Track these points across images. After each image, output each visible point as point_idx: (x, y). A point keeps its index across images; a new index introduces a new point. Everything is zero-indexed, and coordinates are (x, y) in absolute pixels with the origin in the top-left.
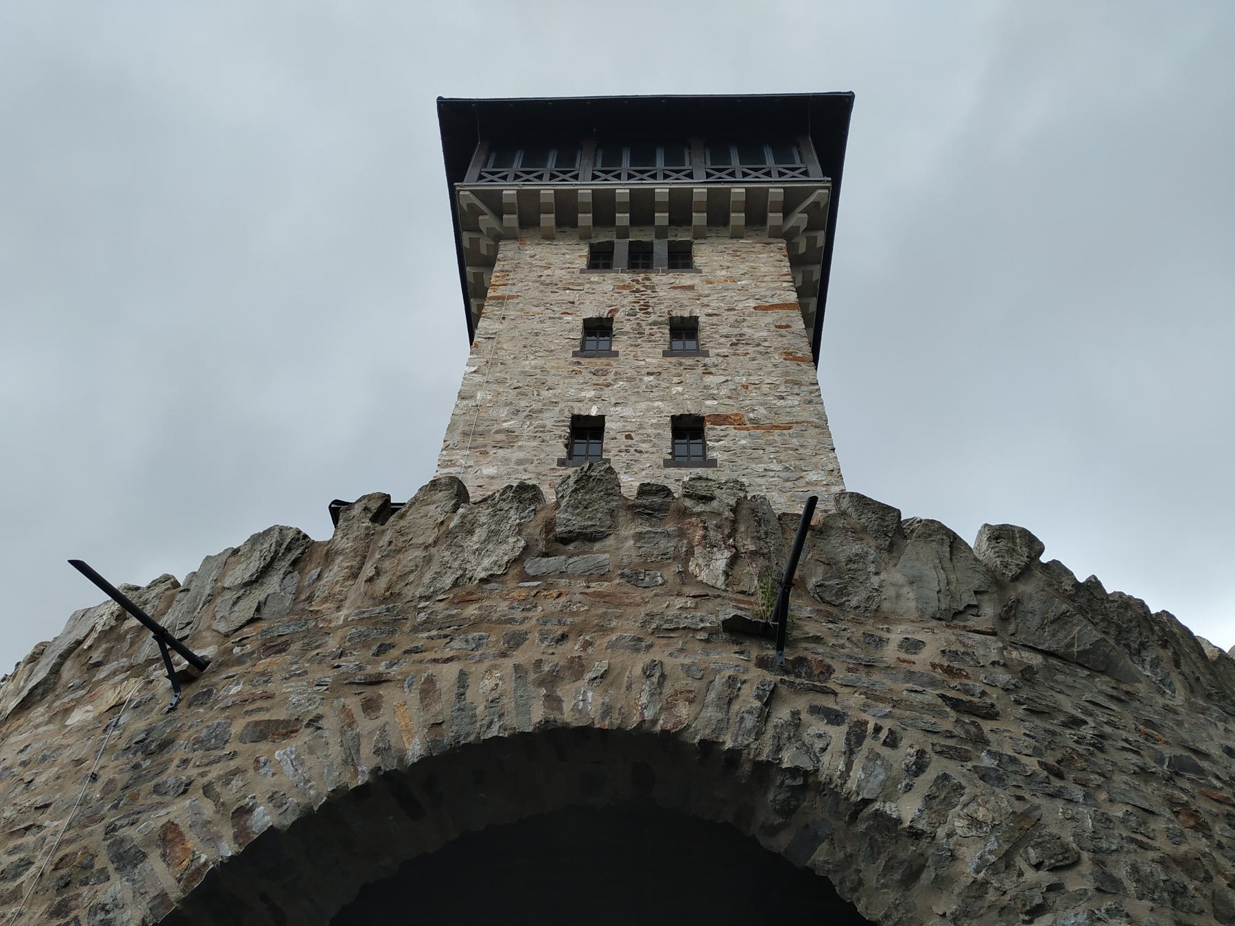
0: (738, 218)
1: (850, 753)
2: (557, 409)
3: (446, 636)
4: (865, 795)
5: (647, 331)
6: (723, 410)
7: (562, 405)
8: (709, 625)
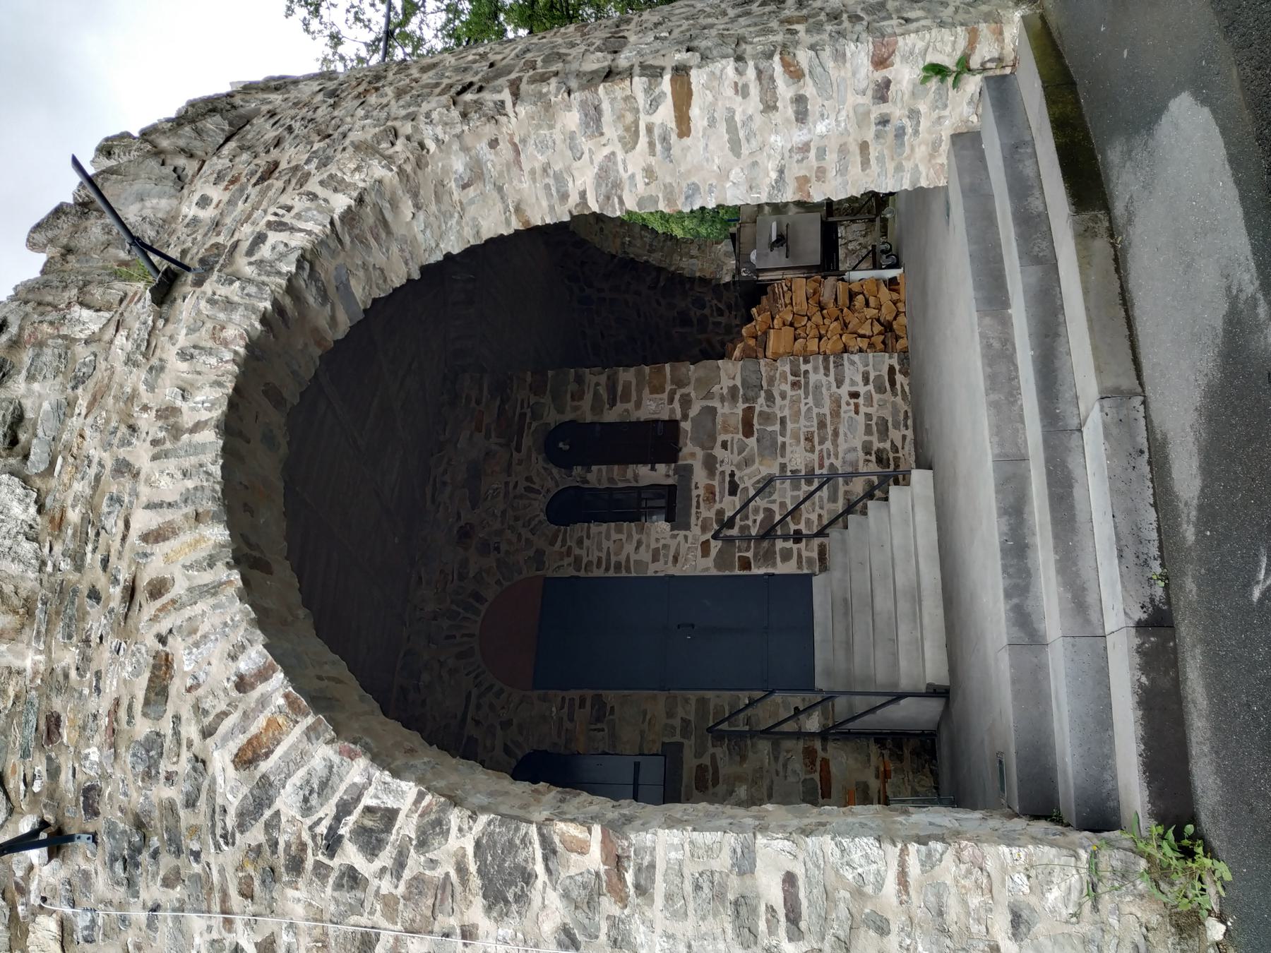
1: (292, 229)
3: (98, 534)
8: (151, 318)
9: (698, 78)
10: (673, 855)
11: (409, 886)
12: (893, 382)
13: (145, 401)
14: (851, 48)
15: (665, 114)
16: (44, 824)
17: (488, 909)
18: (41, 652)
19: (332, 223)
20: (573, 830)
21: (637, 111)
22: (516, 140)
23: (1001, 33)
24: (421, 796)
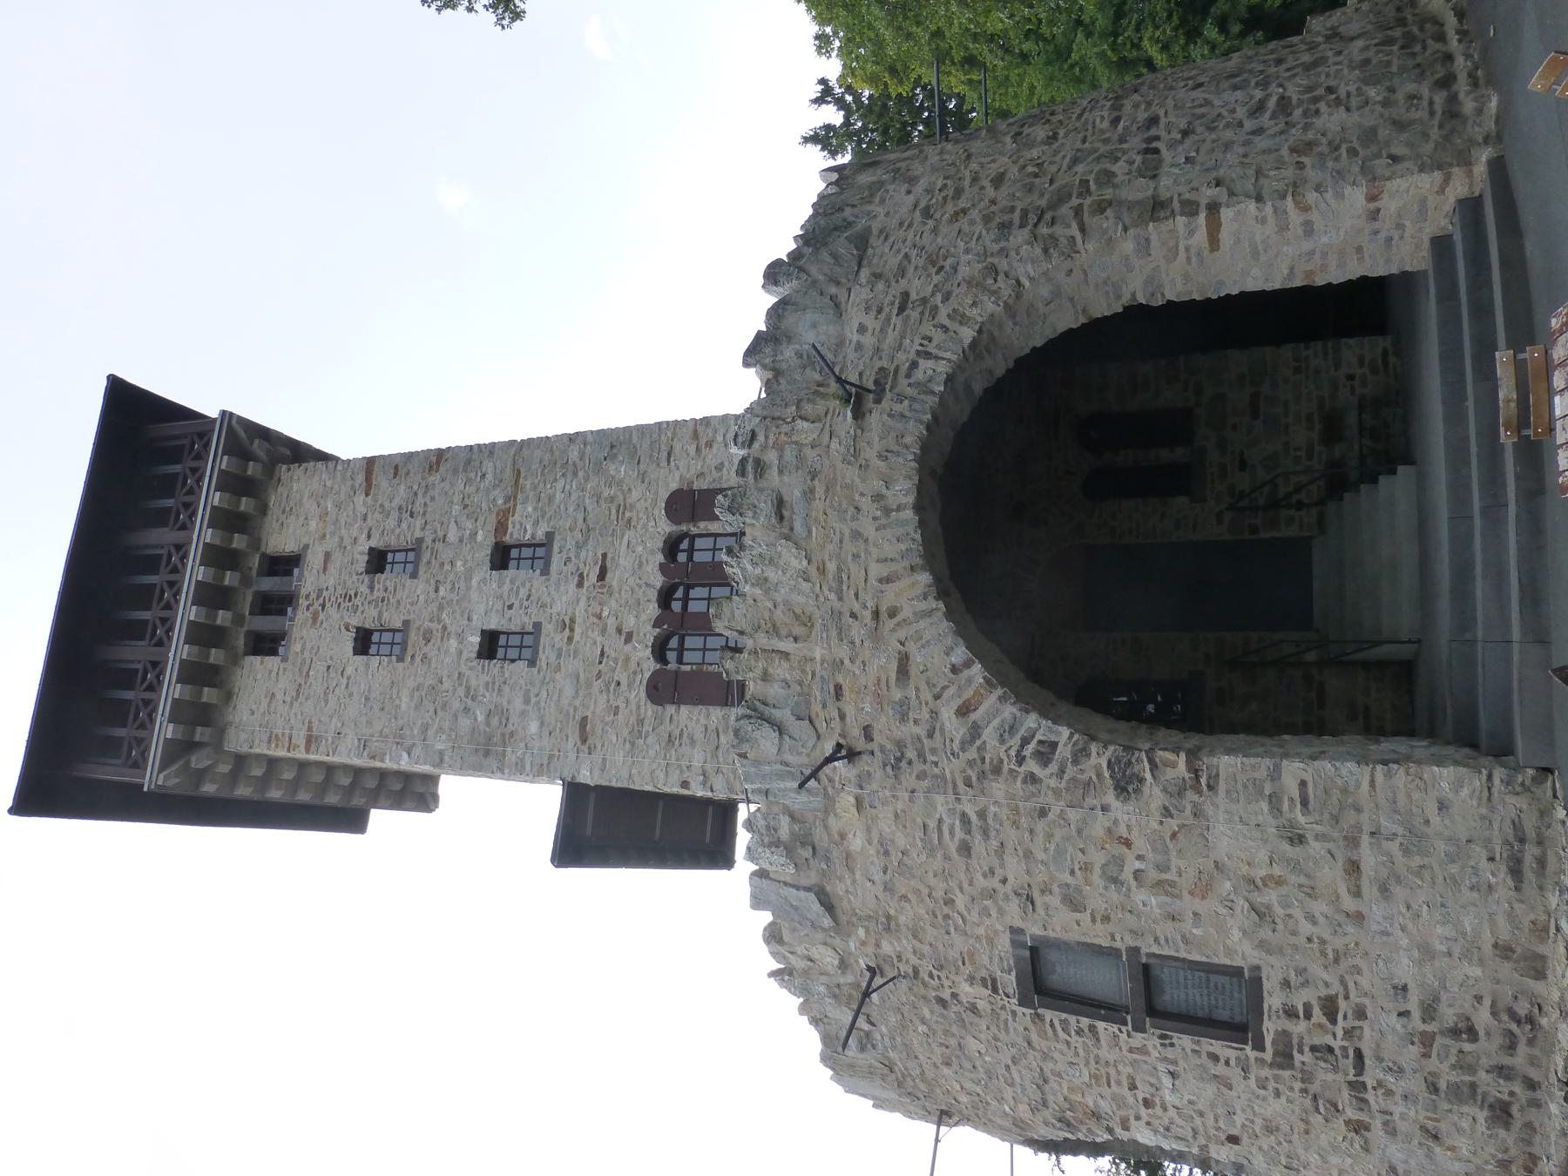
0: (245, 504)
1: (937, 358)
2: (468, 673)
4: (960, 352)
5: (382, 594)
6: (491, 526)
7: (463, 669)
9: (1226, 214)
10: (1231, 769)
11: (1068, 782)
12: (1386, 364)
13: (861, 490)
14: (1348, 190)
15: (1201, 236)
16: (839, 746)
17: (1117, 797)
18: (825, 649)
19: (963, 352)
20: (1169, 756)
21: (1178, 238)
22: (1086, 267)
23: (1471, 171)
24: (1072, 735)
